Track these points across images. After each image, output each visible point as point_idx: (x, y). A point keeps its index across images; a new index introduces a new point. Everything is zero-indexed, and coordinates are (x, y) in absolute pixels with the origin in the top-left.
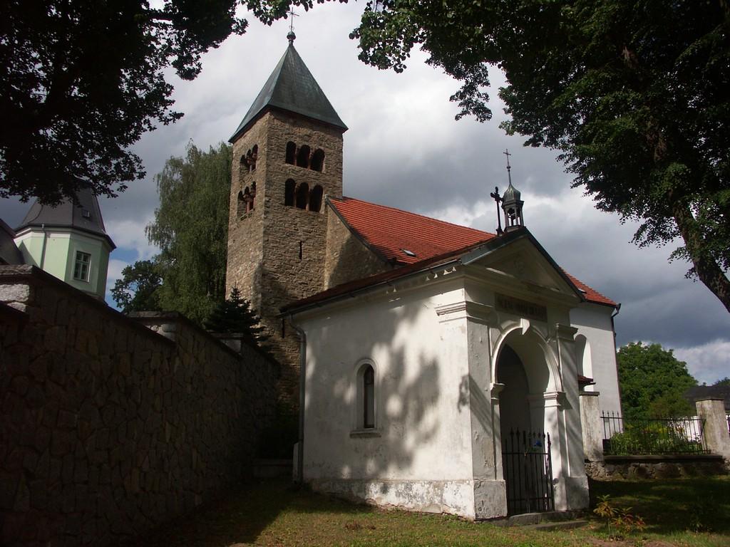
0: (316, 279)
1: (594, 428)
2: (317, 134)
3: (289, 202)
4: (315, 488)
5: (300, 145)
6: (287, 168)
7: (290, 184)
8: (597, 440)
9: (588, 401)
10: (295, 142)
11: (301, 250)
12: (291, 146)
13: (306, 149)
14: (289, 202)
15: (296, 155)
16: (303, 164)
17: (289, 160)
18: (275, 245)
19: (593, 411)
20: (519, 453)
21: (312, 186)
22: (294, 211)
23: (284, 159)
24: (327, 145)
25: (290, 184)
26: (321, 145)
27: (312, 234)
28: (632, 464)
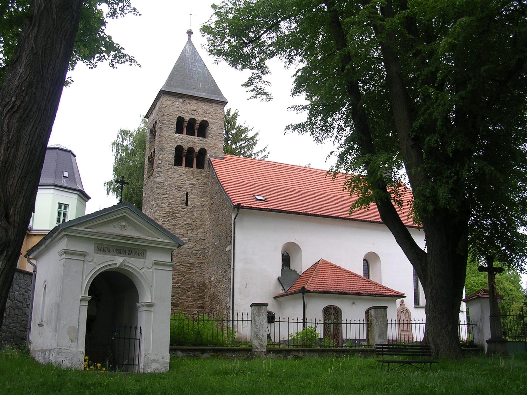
0: (199, 221)
1: (261, 328)
2: (203, 106)
3: (178, 162)
4: (32, 354)
5: (188, 119)
6: (176, 137)
7: (179, 149)
8: (263, 337)
9: (258, 310)
10: (184, 117)
11: (187, 199)
12: (180, 121)
13: (192, 121)
14: (178, 162)
15: (184, 126)
16: (191, 132)
17: (179, 130)
18: (166, 196)
19: (261, 317)
20: (124, 338)
21: (197, 150)
22: (182, 169)
23: (174, 131)
24: (211, 117)
25: (179, 149)
26: (205, 117)
27: (196, 186)
28: (292, 353)
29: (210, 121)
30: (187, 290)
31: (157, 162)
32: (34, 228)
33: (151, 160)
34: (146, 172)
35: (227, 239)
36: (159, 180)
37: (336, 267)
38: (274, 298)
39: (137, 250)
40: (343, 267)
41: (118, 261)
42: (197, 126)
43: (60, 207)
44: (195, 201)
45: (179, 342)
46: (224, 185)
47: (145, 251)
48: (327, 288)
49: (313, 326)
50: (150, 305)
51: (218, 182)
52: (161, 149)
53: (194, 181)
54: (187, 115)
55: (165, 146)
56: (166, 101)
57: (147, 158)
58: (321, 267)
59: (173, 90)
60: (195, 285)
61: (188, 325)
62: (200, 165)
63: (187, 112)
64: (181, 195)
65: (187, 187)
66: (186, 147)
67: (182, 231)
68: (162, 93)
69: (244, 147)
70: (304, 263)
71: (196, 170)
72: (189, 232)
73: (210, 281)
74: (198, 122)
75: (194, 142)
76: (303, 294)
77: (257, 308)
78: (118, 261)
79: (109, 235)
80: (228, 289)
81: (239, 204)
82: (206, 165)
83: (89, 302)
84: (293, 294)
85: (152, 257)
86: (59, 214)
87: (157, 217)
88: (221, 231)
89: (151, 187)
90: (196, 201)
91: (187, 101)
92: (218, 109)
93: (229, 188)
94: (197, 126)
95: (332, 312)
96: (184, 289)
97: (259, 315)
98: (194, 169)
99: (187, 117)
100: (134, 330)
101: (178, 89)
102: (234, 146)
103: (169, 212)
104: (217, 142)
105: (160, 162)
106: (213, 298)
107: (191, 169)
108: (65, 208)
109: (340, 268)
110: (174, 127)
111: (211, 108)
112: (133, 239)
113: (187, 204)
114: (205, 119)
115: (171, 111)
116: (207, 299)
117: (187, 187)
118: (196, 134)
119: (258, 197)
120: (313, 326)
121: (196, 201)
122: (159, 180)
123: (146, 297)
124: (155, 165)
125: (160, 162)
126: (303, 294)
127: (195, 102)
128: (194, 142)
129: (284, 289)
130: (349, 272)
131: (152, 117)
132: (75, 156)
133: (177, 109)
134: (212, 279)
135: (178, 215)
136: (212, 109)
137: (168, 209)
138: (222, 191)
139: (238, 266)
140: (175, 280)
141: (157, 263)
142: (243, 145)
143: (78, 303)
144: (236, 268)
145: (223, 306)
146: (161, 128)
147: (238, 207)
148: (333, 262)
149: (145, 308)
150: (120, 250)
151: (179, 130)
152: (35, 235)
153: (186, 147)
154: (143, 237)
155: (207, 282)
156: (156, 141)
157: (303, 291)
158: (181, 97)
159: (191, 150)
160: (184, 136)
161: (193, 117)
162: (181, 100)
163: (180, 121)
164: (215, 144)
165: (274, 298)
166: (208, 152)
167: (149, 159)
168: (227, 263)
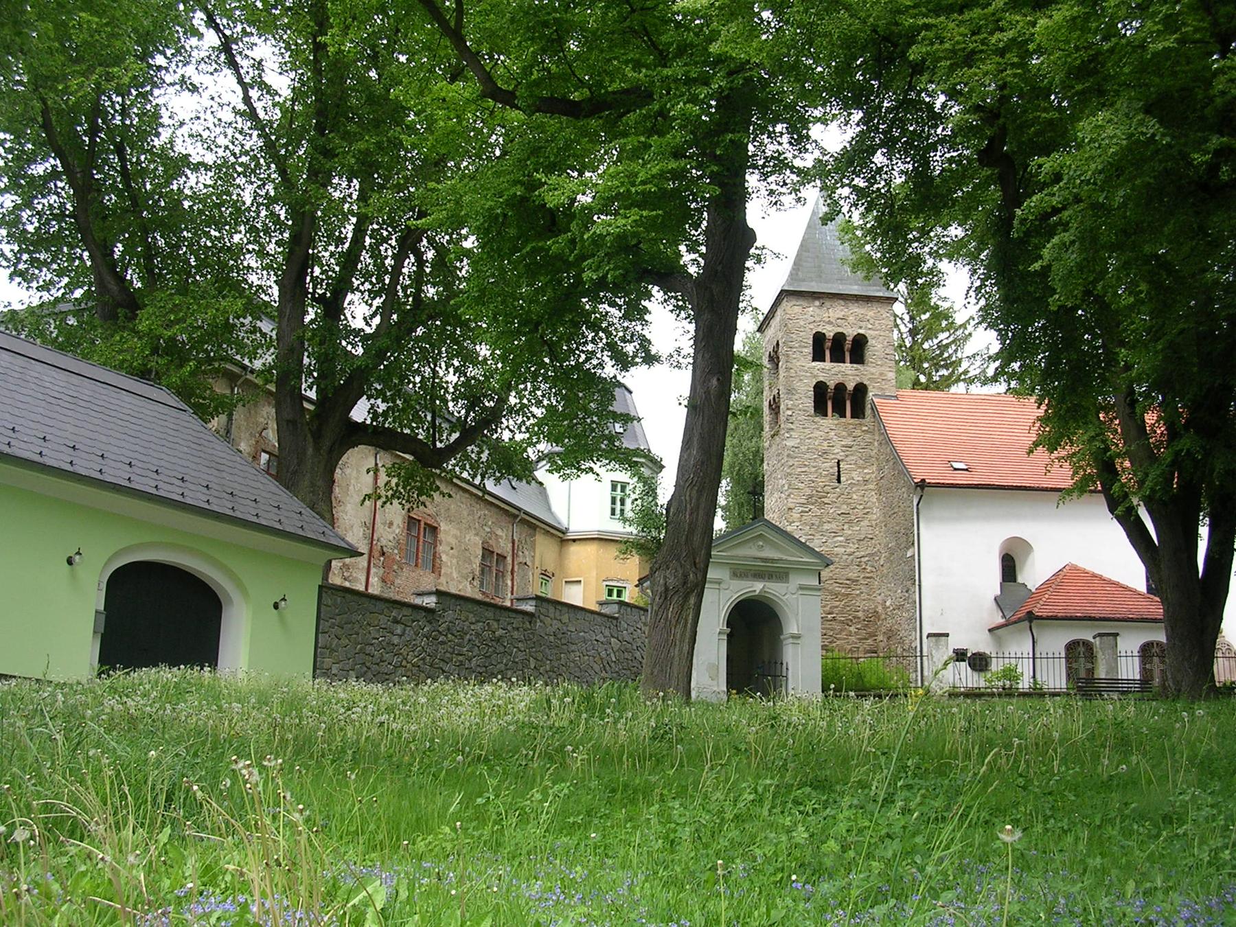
2: (856, 310)
3: (820, 408)
12: (819, 339)
13: (839, 338)
16: (838, 357)
17: (818, 356)
21: (850, 386)
22: (830, 421)
25: (820, 388)
29: (868, 334)
30: (848, 623)
31: (784, 413)
32: (571, 529)
33: (775, 407)
34: (767, 427)
35: (907, 539)
36: (789, 443)
37: (1094, 575)
38: (990, 630)
39: (777, 573)
40: (1106, 575)
41: (758, 587)
42: (848, 345)
43: (614, 488)
44: (852, 475)
45: (836, 683)
46: (899, 447)
47: (787, 575)
48: (1072, 612)
49: (1013, 661)
50: (797, 637)
51: (887, 441)
52: (790, 391)
53: (848, 441)
54: (829, 327)
55: (797, 384)
56: (791, 308)
57: (766, 404)
58: (1069, 576)
59: (803, 288)
60: (860, 614)
61: (845, 665)
62: (858, 412)
63: (830, 323)
64: (829, 466)
65: (838, 452)
66: (832, 384)
67: (833, 526)
68: (784, 295)
69: (947, 346)
70: (1034, 574)
71: (852, 421)
72: (846, 527)
73: (885, 608)
74: (850, 338)
75: (844, 373)
76: (1031, 622)
77: (933, 639)
78: (758, 587)
79: (745, 558)
80: (912, 618)
81: (923, 480)
82: (868, 412)
83: (728, 635)
84: (1015, 622)
85: (796, 580)
86: (613, 501)
87: (791, 505)
88: (898, 524)
89: (778, 455)
90: (854, 474)
91: (828, 304)
92: (882, 311)
93: (908, 452)
94: (848, 345)
95: (1082, 649)
96: (842, 622)
97: (938, 649)
98: (849, 418)
99: (830, 331)
100: (778, 665)
101: (813, 284)
102: (926, 346)
103: (811, 496)
104: (885, 369)
105: (789, 413)
106: (891, 634)
107: (843, 420)
108: (623, 489)
109: (1101, 578)
110: (809, 404)
111: (870, 312)
112: (773, 560)
113: (839, 481)
114: (861, 331)
115: (802, 323)
116: (880, 638)
117: (838, 452)
118: (848, 358)
119: (956, 465)
120: (1013, 661)
121: (854, 474)
122: (789, 443)
123: (791, 627)
124: (782, 418)
125: (789, 413)
126: (1031, 622)
127: (842, 302)
128: (844, 373)
129: (1004, 616)
130: (1117, 584)
131: (770, 332)
132: (631, 392)
133: (812, 319)
134: (888, 604)
135: (826, 500)
136: (871, 313)
137: (808, 492)
138: (895, 459)
139: (929, 580)
140: (827, 609)
141: (802, 588)
142: (944, 342)
143: (716, 636)
144: (923, 584)
145: (906, 647)
146: (788, 356)
147: (922, 485)
148: (1088, 568)
149: (791, 640)
150: (759, 575)
151: (818, 356)
152: (574, 540)
153: (832, 384)
154: (785, 557)
155: (880, 609)
156: (781, 377)
157: (1031, 617)
158: (818, 298)
159: (840, 387)
160: (827, 365)
161: (840, 330)
162: (817, 303)
163: (819, 339)
164: (881, 374)
165: (990, 630)
166: (870, 388)
167: (770, 405)
168: (910, 577)
